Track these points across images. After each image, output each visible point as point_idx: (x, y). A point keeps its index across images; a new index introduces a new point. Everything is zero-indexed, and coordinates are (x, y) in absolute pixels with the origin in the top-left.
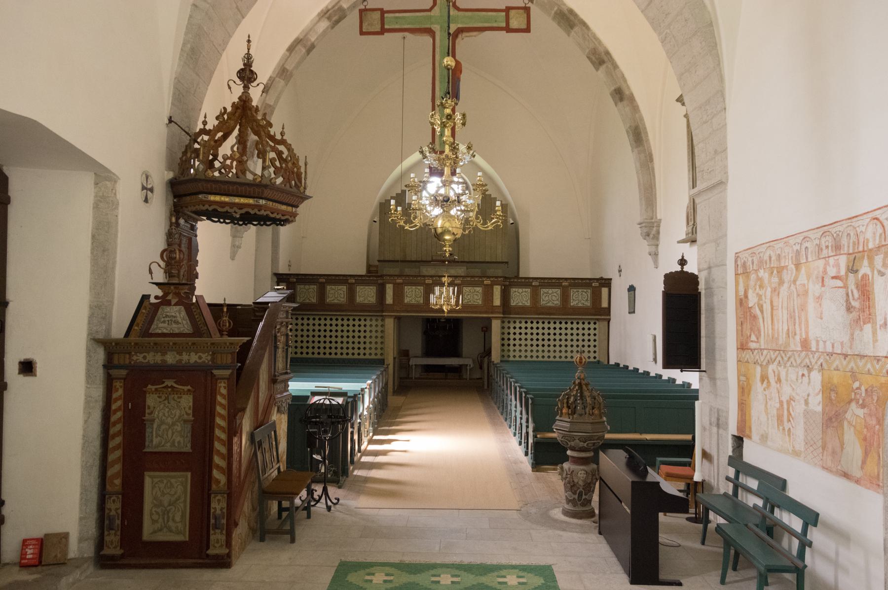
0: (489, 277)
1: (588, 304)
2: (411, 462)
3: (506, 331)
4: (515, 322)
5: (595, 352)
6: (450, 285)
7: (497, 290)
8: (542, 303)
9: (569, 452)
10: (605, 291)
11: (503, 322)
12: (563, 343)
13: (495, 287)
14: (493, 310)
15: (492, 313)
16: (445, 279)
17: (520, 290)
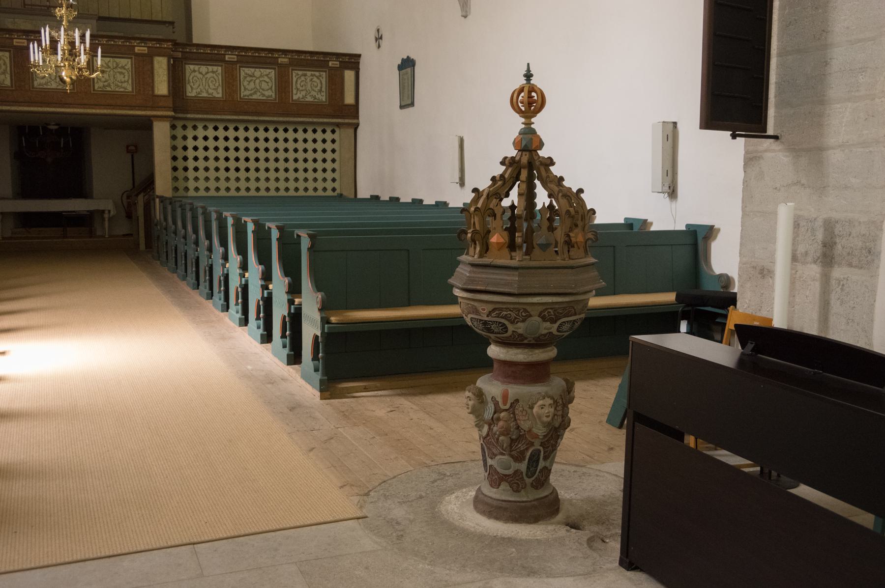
0: (143, 40)
1: (323, 97)
2: (18, 405)
3: (180, 143)
4: (195, 128)
5: (334, 180)
6: (72, 25)
7: (161, 66)
8: (244, 93)
9: (494, 351)
10: (349, 75)
11: (173, 127)
12: (281, 165)
13: (157, 59)
14: (154, 101)
15: (153, 108)
16: (61, 12)
17: (203, 69)
